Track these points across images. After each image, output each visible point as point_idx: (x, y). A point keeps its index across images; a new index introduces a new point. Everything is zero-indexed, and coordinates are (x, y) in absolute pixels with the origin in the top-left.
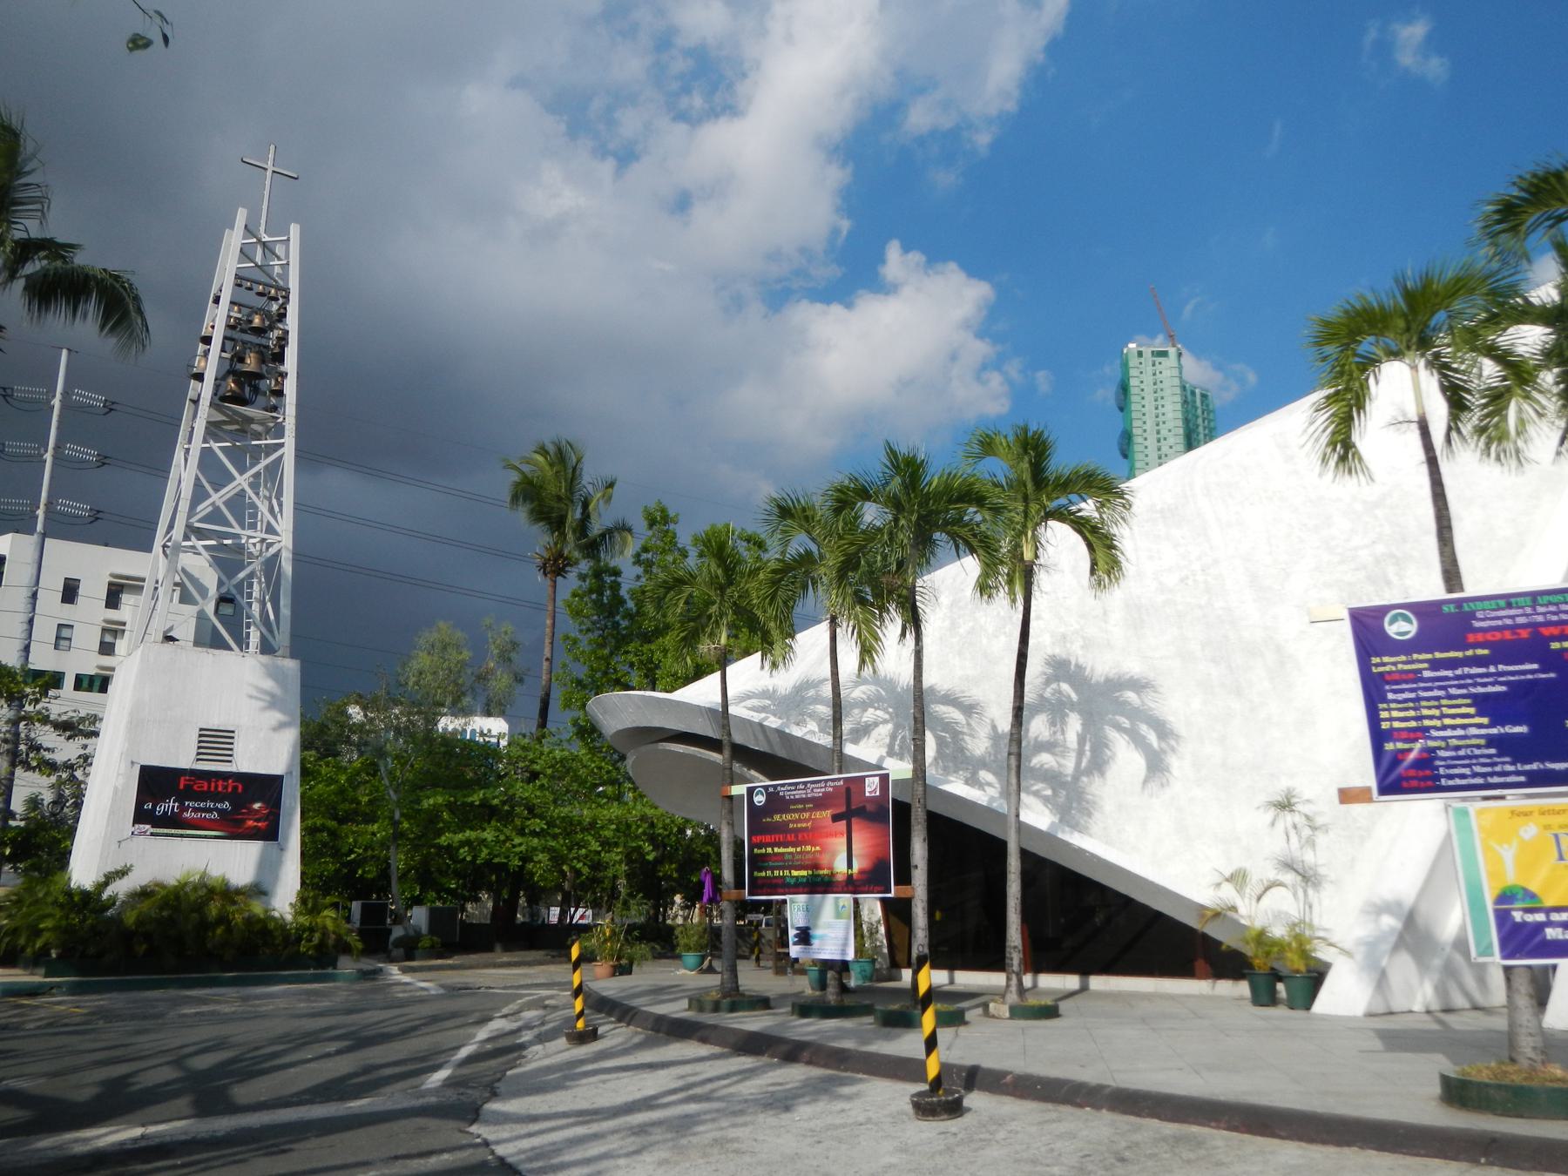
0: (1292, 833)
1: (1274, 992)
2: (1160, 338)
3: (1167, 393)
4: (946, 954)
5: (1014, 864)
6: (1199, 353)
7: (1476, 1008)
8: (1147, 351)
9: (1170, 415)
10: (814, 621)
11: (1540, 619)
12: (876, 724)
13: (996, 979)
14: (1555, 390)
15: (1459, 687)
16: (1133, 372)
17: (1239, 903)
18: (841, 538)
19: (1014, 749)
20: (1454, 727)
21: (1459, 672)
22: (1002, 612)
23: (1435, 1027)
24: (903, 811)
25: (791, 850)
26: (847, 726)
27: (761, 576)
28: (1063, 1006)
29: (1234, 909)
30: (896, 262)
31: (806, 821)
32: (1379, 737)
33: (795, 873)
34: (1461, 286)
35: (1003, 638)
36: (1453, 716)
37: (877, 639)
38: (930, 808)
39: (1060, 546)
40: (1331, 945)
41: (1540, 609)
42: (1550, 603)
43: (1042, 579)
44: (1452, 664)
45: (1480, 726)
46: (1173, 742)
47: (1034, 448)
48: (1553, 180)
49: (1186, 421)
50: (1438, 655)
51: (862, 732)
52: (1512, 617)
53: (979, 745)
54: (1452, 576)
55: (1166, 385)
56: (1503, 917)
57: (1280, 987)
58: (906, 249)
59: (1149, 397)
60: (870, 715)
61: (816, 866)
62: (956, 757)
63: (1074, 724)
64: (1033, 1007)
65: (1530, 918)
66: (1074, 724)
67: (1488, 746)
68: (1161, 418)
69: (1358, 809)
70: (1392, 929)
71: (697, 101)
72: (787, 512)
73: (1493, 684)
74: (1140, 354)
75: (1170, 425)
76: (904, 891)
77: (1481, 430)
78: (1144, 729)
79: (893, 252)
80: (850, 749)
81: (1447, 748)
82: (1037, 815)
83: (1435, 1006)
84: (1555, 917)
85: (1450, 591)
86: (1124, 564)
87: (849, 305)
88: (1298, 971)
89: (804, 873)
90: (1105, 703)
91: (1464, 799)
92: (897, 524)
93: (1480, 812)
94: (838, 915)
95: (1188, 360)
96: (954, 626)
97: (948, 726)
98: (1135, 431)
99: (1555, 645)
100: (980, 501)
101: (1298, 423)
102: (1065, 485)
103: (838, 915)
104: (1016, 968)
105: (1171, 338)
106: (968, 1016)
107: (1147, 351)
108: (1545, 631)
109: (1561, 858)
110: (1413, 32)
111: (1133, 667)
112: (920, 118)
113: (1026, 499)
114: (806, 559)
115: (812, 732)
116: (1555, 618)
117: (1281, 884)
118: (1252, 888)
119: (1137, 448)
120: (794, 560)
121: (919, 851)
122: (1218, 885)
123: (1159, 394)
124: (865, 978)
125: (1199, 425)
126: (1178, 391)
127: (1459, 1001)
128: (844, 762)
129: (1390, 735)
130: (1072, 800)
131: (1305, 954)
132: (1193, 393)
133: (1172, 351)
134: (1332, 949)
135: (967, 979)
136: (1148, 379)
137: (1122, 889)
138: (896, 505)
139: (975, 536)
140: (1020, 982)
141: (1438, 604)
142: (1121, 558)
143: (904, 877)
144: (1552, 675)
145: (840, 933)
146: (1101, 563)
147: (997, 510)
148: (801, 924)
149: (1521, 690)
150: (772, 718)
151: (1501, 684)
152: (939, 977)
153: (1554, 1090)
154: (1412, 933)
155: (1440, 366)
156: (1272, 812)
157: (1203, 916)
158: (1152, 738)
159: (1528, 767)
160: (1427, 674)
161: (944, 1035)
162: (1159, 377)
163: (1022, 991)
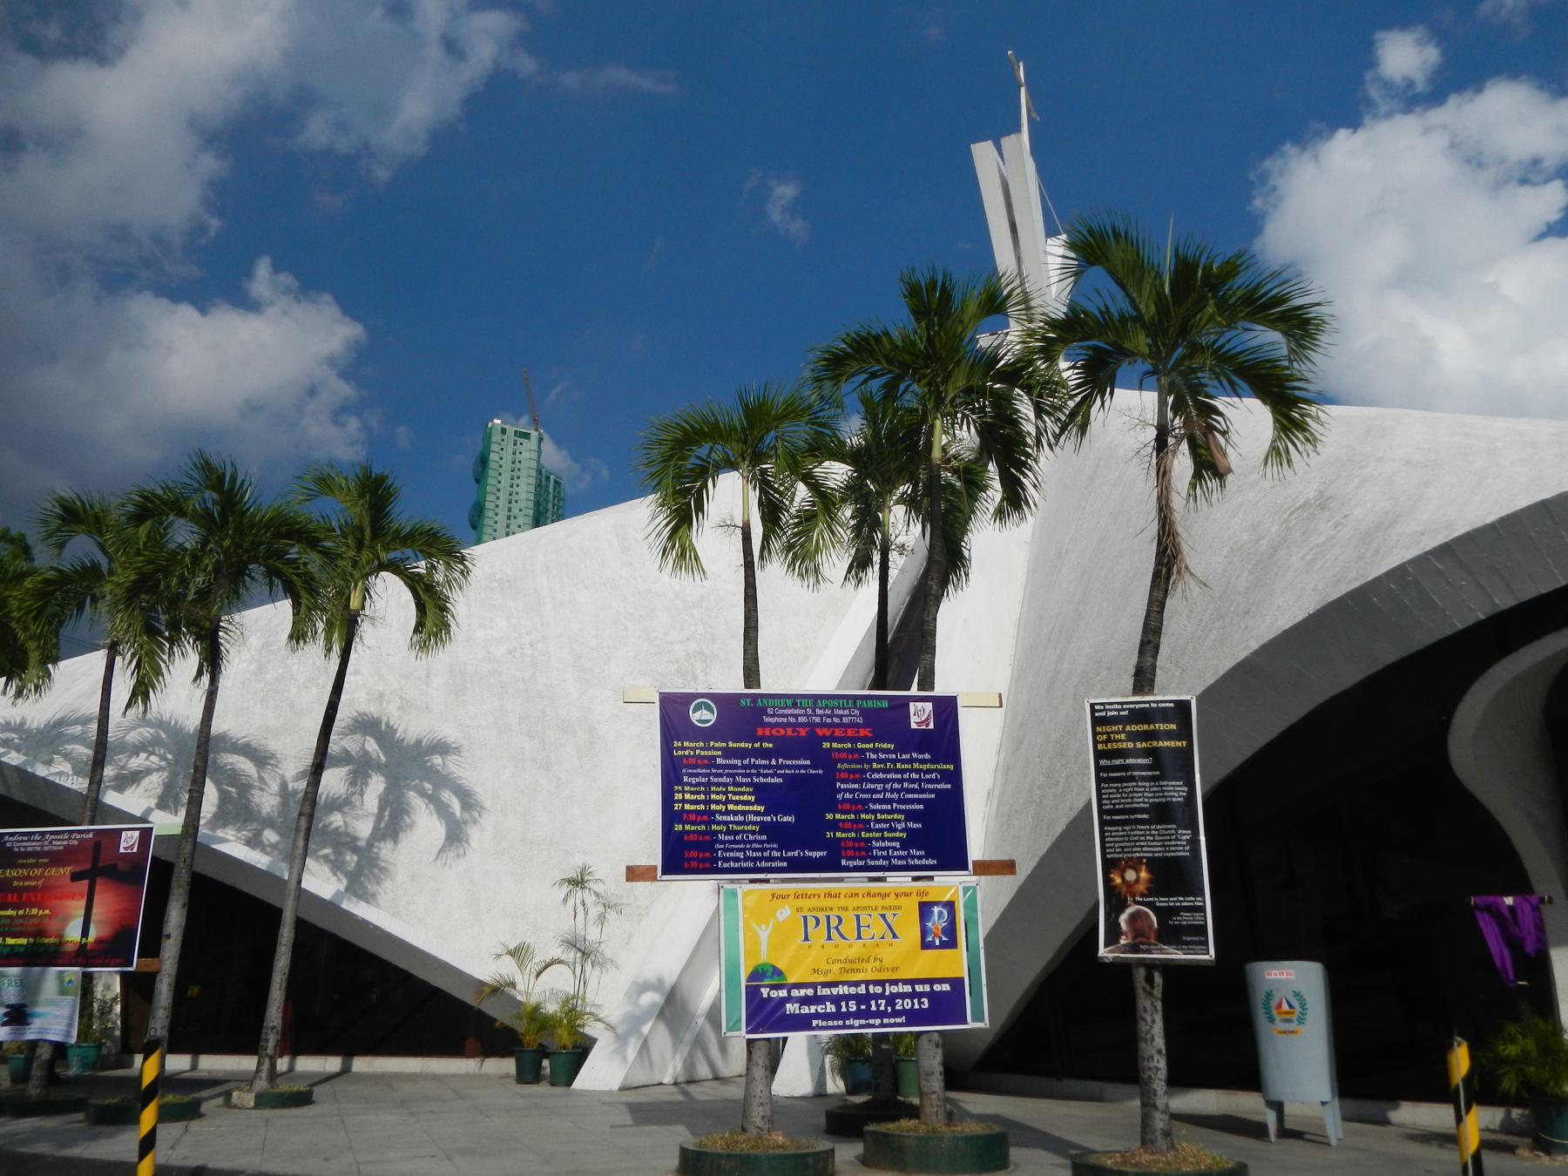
0: (580, 909)
1: (539, 1067)
2: (525, 419)
3: (524, 473)
4: (184, 1038)
5: (286, 934)
6: (559, 442)
7: (716, 1078)
8: (511, 430)
9: (523, 496)
10: (89, 647)
11: (818, 720)
12: (149, 772)
13: (247, 1063)
14: (852, 523)
15: (744, 775)
16: (494, 447)
17: (519, 980)
18: (138, 554)
19: (307, 810)
20: (736, 813)
21: (746, 762)
22: (315, 662)
23: (680, 1098)
24: (163, 870)
25: (10, 912)
26: (109, 771)
27: (28, 583)
28: (318, 1091)
29: (513, 985)
30: (263, 278)
31: (36, 878)
32: (670, 815)
33: (10, 941)
34: (792, 411)
35: (314, 690)
36: (736, 803)
37: (158, 673)
38: (198, 868)
39: (389, 600)
40: (599, 1020)
41: (819, 712)
42: (827, 707)
43: (365, 629)
44: (741, 754)
45: (757, 813)
46: (476, 814)
47: (376, 492)
48: (872, 342)
49: (537, 504)
50: (731, 744)
51: (127, 780)
52: (796, 716)
53: (267, 801)
54: (751, 673)
55: (524, 465)
56: (752, 992)
57: (546, 1063)
58: (277, 268)
59: (506, 475)
60: (138, 762)
61: (40, 933)
62: (237, 810)
63: (376, 785)
64: (282, 1094)
65: (774, 994)
66: (376, 785)
67: (760, 833)
68: (514, 497)
69: (641, 887)
70: (653, 1005)
71: (53, 32)
72: (73, 516)
73: (772, 776)
74: (504, 431)
75: (522, 505)
76: (150, 964)
77: (790, 547)
78: (448, 797)
79: (263, 268)
80: (111, 798)
81: (728, 832)
82: (321, 882)
83: (681, 1079)
84: (795, 993)
85: (747, 687)
86: (453, 628)
87: (203, 311)
88: (564, 1047)
89: (23, 941)
90: (411, 766)
91: (732, 881)
92: (202, 548)
93: (746, 894)
94: (63, 991)
95: (548, 446)
96: (261, 670)
97: (234, 777)
98: (487, 505)
99: (826, 745)
100: (310, 540)
101: (641, 517)
102: (408, 539)
103: (63, 991)
104: (270, 1051)
105: (536, 422)
106: (204, 1108)
107: (511, 430)
108: (820, 732)
109: (806, 939)
110: (786, 191)
111: (448, 732)
112: (316, 131)
113: (360, 546)
114: (91, 573)
115: (64, 773)
117: (561, 962)
118: (533, 966)
119: (487, 522)
120: (76, 572)
121: (175, 917)
122: (499, 956)
123: (516, 473)
124: (85, 1066)
125: (548, 507)
126: (534, 473)
127: (703, 1071)
128: (94, 807)
129: (681, 816)
130: (364, 870)
131: (573, 1028)
132: (548, 479)
133: (534, 434)
134: (600, 1025)
135: (212, 1064)
136: (508, 456)
137: (402, 964)
138: (204, 519)
139: (298, 575)
140: (273, 1066)
141: (736, 698)
142: (451, 622)
143: (152, 948)
145: (66, 1012)
146: (429, 623)
147: (330, 556)
148: (13, 1000)
149: (794, 782)
150: (14, 754)
151: (779, 776)
152: (178, 1063)
153: (775, 1156)
154: (673, 1007)
155: (764, 485)
156: (565, 889)
157: (480, 992)
158: (456, 805)
159: (790, 854)
160: (719, 761)
161: (169, 1133)
162: (519, 455)
163: (273, 1075)
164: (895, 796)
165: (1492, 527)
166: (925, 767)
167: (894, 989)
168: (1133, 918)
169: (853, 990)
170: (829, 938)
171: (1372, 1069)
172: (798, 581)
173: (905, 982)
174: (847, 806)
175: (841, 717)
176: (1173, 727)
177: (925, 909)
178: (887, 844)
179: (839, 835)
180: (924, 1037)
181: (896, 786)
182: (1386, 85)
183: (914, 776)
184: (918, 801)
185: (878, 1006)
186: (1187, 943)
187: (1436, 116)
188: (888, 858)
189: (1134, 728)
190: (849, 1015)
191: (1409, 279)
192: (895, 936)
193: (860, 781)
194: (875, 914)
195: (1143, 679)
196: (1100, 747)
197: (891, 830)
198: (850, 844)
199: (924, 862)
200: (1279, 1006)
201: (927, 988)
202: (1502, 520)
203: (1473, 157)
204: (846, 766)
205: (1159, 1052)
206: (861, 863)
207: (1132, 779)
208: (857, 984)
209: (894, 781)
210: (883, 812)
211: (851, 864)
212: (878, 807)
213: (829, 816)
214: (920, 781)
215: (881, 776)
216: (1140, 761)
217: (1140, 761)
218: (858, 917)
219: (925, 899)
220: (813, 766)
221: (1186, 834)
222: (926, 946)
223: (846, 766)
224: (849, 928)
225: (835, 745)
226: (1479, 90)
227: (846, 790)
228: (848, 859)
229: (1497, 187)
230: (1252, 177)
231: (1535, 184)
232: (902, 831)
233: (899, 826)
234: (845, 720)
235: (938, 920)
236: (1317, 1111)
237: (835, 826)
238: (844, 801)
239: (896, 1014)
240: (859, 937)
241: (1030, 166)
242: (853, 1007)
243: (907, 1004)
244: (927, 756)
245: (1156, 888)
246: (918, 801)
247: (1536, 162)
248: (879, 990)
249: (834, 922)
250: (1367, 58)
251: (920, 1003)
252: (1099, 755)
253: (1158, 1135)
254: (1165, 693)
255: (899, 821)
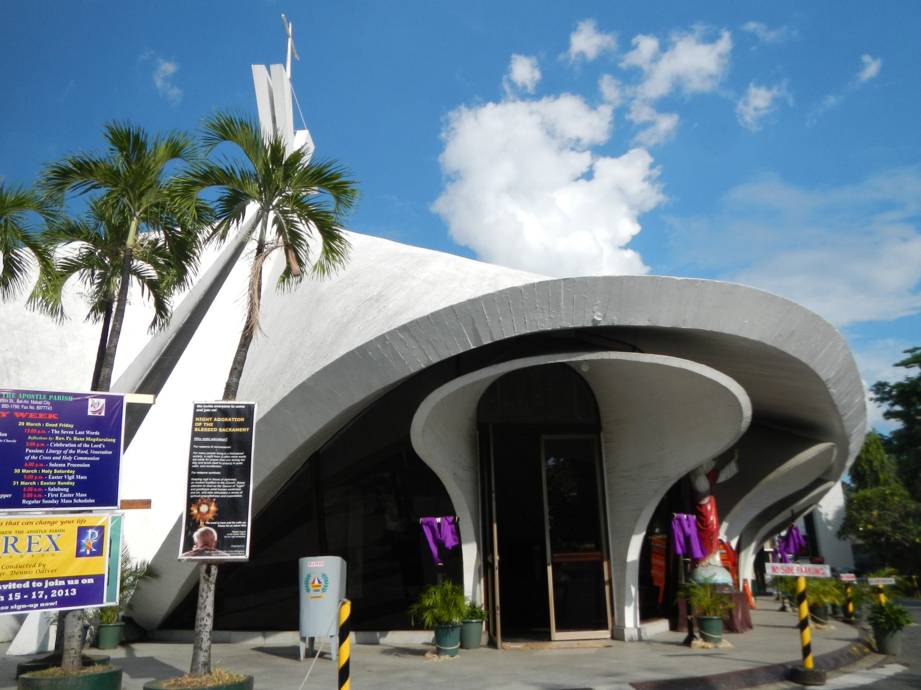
11: (17, 407)
42: (26, 398)
99: (21, 424)
116: (26, 408)
144: (14, 441)
164: (70, 458)
165: (427, 318)
166: (94, 440)
167: (52, 584)
168: (204, 534)
169: (19, 586)
170: (6, 551)
171: (371, 612)
172: (49, 318)
173: (60, 579)
174: (31, 464)
175: (35, 406)
176: (243, 419)
177: (82, 532)
178: (59, 489)
179: (22, 483)
180: (70, 615)
181: (71, 452)
182: (513, 85)
183: (86, 445)
184: (87, 462)
185: (37, 595)
186: (234, 549)
187: (535, 106)
188: (59, 498)
189: (219, 420)
190: (14, 602)
191: (514, 190)
192: (57, 549)
193: (44, 448)
194: (44, 535)
195: (231, 390)
196: (196, 430)
197: (63, 480)
198: (31, 489)
199: (86, 501)
200: (313, 582)
201: (77, 582)
202: (432, 314)
203: (550, 131)
204: (35, 438)
205: (208, 615)
206: (38, 502)
207: (213, 450)
208: (23, 582)
209: (70, 448)
210: (58, 468)
211: (30, 502)
212: (56, 465)
213: (17, 471)
214: (89, 449)
215: (61, 445)
216: (220, 440)
217: (220, 440)
218: (30, 538)
219: (83, 525)
220: (9, 438)
221: (242, 484)
222: (79, 554)
223: (35, 438)
224: (22, 544)
225: (28, 424)
226: (557, 97)
227: (32, 453)
228: (27, 499)
229: (561, 149)
230: (442, 119)
231: (578, 152)
232: (72, 481)
233: (70, 478)
234: (38, 408)
235: (90, 539)
236: (329, 640)
237: (21, 477)
238: (30, 460)
239: (53, 600)
240: (29, 550)
241: (288, 86)
242: (18, 596)
243: (60, 593)
244: (97, 433)
245: (219, 516)
246: (87, 462)
247: (578, 140)
248: (40, 584)
249: (11, 541)
250: (504, 67)
251: (70, 592)
252: (194, 434)
253: (200, 665)
254: (241, 400)
255: (70, 475)
